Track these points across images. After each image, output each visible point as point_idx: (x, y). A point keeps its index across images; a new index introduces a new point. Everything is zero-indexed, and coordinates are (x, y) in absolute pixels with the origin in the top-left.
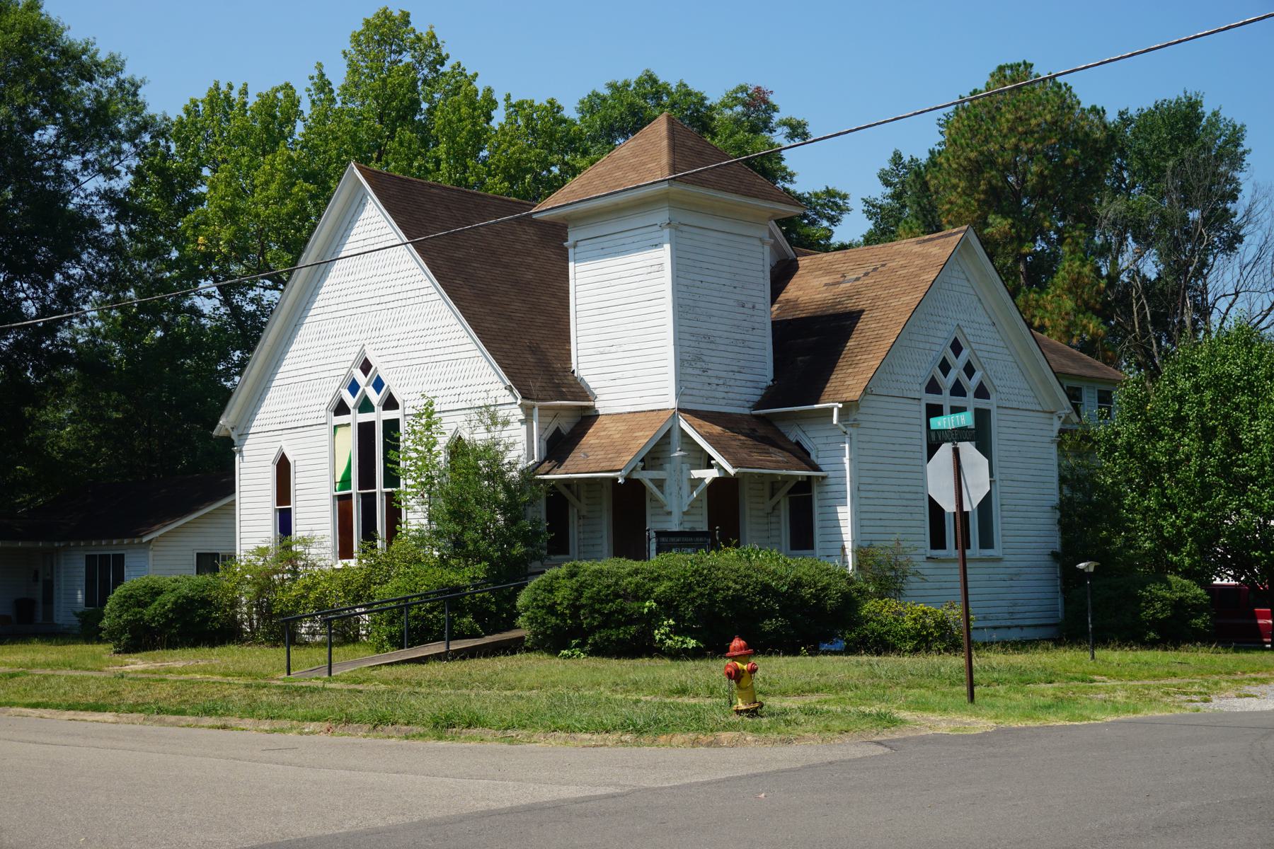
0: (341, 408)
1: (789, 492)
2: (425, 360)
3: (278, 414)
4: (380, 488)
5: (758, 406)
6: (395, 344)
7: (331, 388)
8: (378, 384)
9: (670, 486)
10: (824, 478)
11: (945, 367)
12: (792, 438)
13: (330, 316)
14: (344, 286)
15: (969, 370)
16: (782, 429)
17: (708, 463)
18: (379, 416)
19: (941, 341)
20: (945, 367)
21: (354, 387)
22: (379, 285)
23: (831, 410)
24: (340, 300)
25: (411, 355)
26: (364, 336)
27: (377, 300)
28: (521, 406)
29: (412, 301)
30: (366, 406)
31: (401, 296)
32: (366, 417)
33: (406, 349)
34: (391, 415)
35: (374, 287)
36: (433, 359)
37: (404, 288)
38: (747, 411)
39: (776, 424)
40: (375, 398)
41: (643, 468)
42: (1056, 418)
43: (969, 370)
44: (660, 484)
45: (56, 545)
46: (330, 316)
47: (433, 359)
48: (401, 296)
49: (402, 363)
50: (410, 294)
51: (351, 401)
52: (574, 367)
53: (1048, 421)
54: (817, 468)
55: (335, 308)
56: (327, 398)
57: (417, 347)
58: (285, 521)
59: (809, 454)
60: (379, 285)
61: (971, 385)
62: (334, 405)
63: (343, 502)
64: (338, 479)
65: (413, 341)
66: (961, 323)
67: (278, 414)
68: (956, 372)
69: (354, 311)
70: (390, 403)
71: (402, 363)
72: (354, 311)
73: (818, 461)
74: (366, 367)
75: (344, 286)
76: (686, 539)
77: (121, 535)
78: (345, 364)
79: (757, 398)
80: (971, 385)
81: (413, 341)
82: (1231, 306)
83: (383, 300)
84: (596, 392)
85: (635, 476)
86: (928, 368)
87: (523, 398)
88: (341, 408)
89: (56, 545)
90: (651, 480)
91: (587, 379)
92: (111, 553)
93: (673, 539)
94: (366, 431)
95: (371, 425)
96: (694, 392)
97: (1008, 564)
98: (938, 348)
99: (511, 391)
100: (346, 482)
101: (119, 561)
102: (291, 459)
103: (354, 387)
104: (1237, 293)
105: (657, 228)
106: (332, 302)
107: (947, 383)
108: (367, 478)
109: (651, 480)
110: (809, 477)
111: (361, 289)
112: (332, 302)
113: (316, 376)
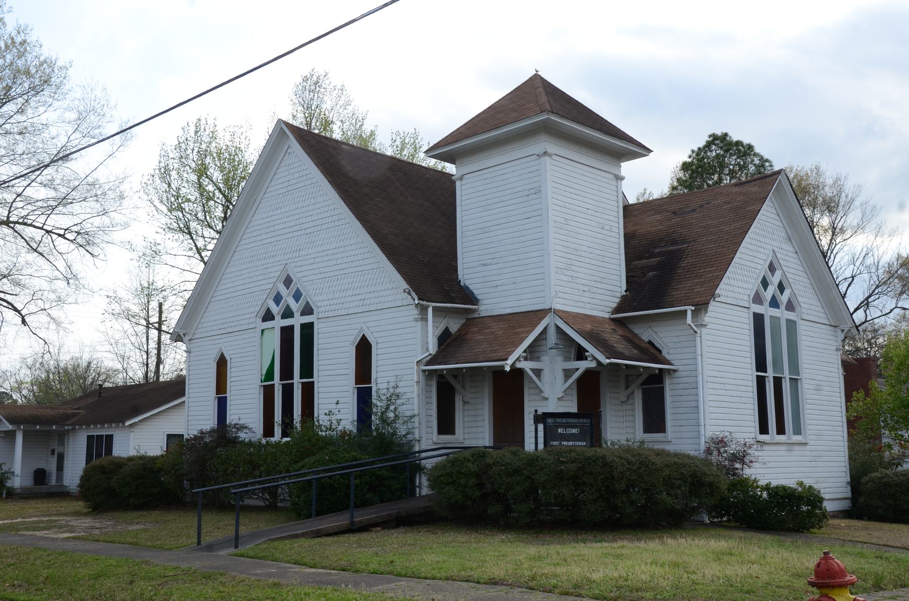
0: (268, 316)
1: (642, 384)
2: (336, 273)
3: (219, 322)
4: (297, 381)
5: (617, 310)
6: (312, 261)
7: (261, 300)
8: (297, 296)
9: (546, 375)
10: (674, 371)
11: (765, 283)
12: (645, 338)
13: (261, 243)
14: (272, 218)
15: (781, 287)
16: (636, 331)
17: (581, 354)
18: (297, 321)
19: (762, 262)
20: (765, 283)
21: (278, 299)
22: (299, 216)
23: (686, 311)
24: (269, 230)
25: (324, 270)
26: (287, 257)
27: (298, 228)
28: (417, 305)
29: (326, 226)
30: (288, 313)
31: (317, 223)
32: (287, 322)
33: (321, 265)
34: (307, 319)
35: (296, 217)
36: (342, 272)
37: (320, 216)
38: (607, 316)
39: (630, 327)
40: (295, 306)
41: (526, 359)
42: (839, 331)
43: (781, 287)
44: (538, 372)
45: (66, 428)
46: (261, 243)
47: (342, 272)
48: (317, 223)
49: (316, 277)
50: (324, 221)
51: (275, 309)
52: (460, 277)
53: (833, 333)
54: (670, 363)
55: (264, 236)
56: (257, 309)
57: (330, 263)
58: (222, 404)
59: (660, 352)
60: (299, 216)
61: (784, 298)
62: (262, 313)
63: (268, 393)
64: (264, 373)
65: (326, 258)
66: (776, 249)
67: (219, 322)
68: (772, 290)
69: (279, 238)
70: (308, 310)
71: (316, 277)
72: (279, 238)
73: (669, 357)
74: (288, 282)
75: (272, 218)
76: (571, 420)
77: (110, 422)
78: (271, 281)
79: (615, 305)
80: (784, 298)
81: (326, 258)
82: (849, 285)
83: (303, 227)
84: (478, 297)
85: (519, 365)
86: (754, 285)
87: (419, 299)
88: (268, 316)
89: (66, 428)
90: (531, 369)
91: (471, 287)
92: (95, 434)
93: (559, 420)
94: (287, 332)
95: (291, 328)
96: (567, 296)
97: (812, 448)
98: (760, 267)
99: (409, 293)
100: (269, 375)
101: (110, 438)
102: (228, 358)
103: (278, 299)
104: (853, 277)
105: (535, 157)
106: (262, 232)
107: (768, 295)
108: (287, 373)
109: (531, 369)
110: (660, 370)
111: (285, 220)
112: (262, 232)
113: (248, 291)
